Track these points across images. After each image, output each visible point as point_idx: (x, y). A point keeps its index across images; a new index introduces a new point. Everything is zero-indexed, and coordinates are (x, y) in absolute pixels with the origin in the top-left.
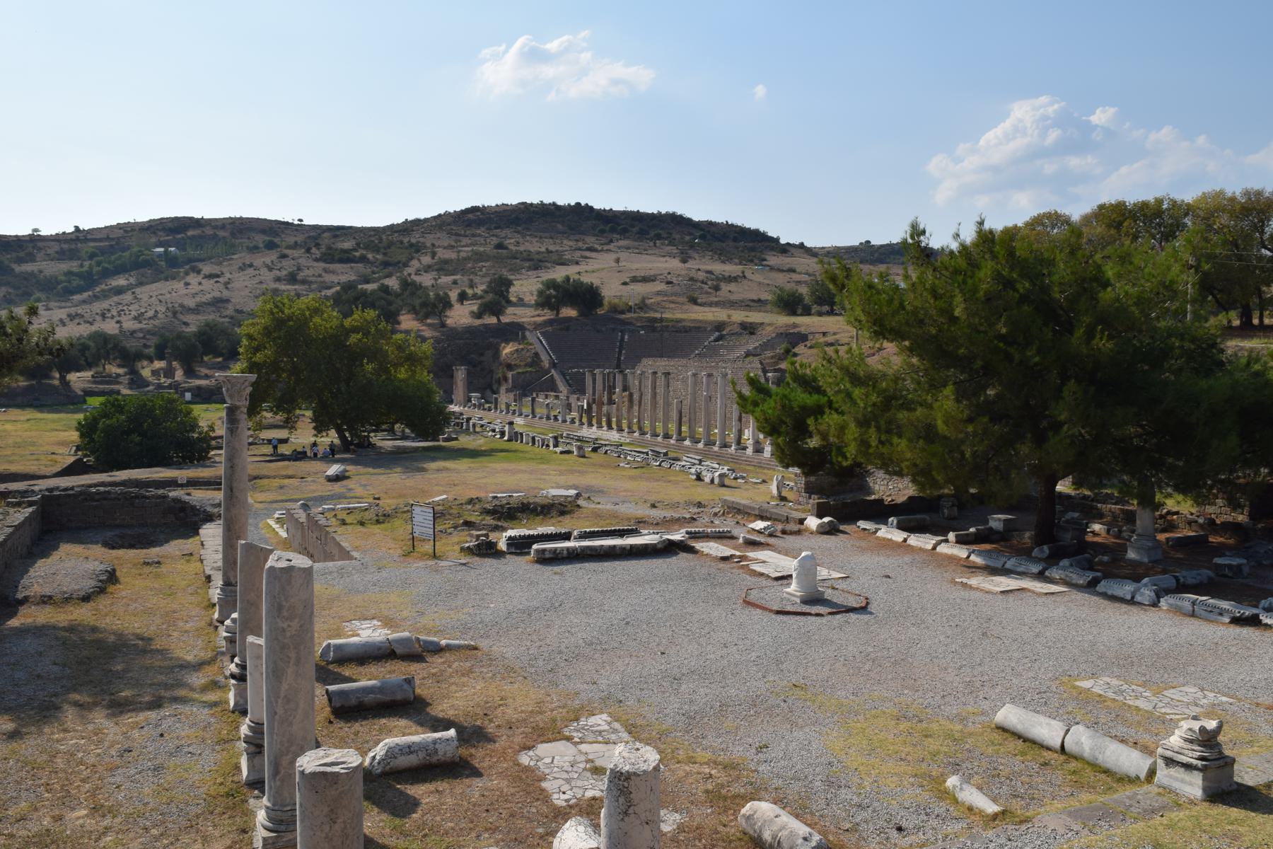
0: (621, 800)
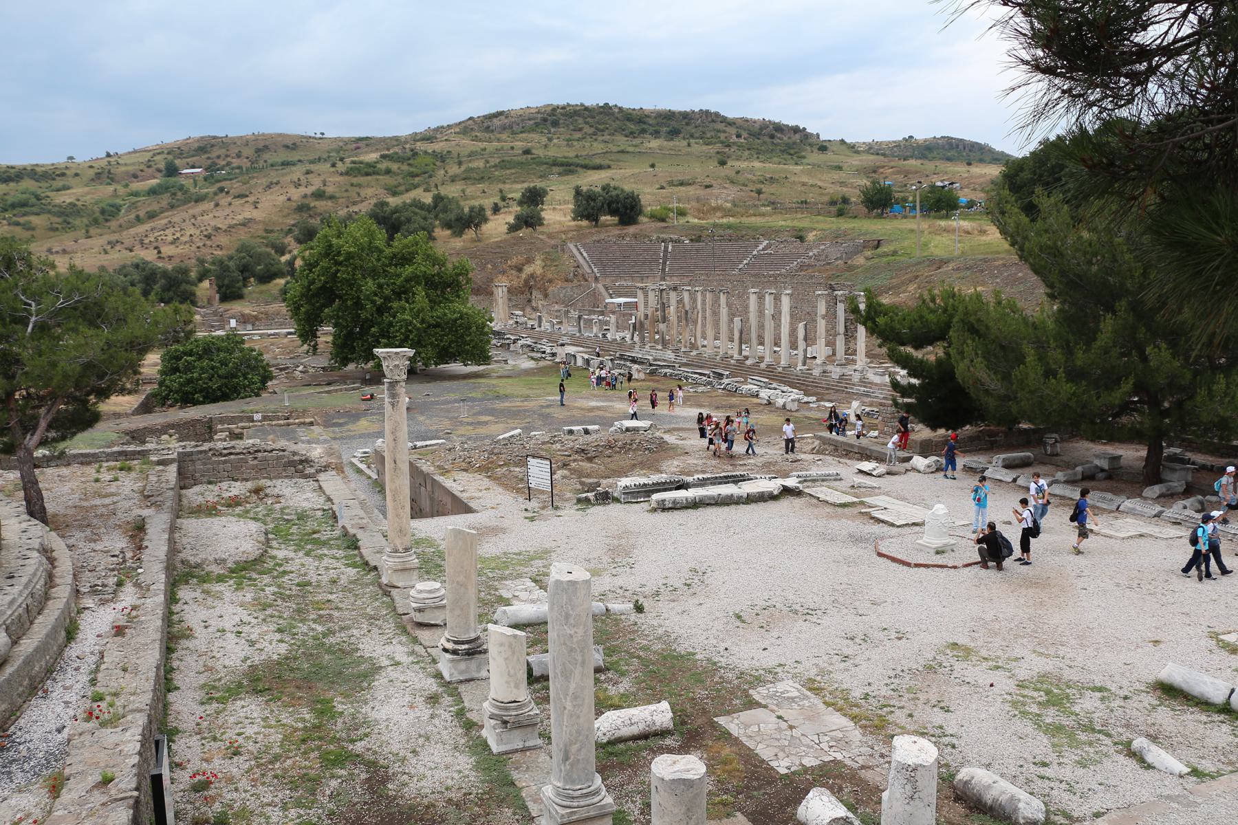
0: (908, 787)
